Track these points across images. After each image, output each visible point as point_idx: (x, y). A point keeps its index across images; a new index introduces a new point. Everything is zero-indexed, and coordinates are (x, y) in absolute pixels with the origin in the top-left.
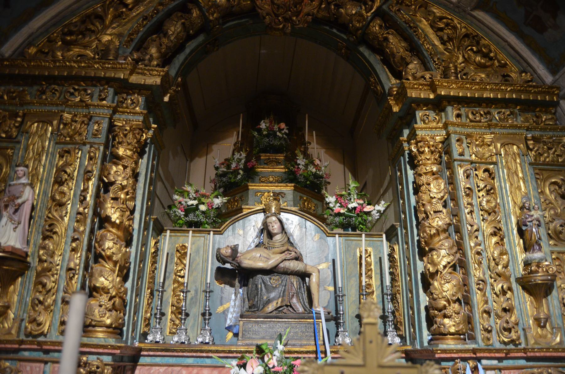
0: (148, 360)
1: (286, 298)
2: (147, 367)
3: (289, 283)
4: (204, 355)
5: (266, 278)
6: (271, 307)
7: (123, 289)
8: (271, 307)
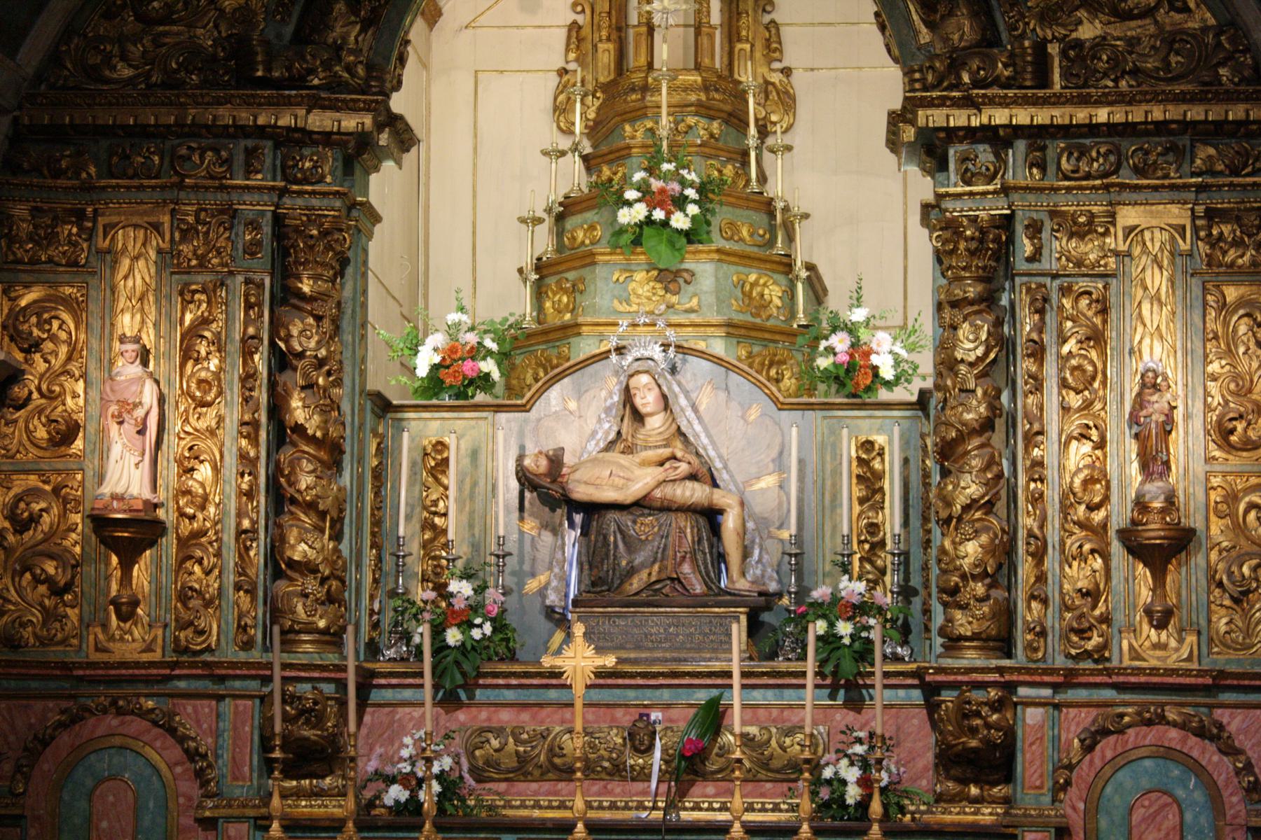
0: (388, 695)
1: (670, 563)
2: (387, 710)
3: (674, 532)
4: (501, 681)
5: (626, 519)
6: (636, 583)
7: (340, 562)
8: (636, 583)
